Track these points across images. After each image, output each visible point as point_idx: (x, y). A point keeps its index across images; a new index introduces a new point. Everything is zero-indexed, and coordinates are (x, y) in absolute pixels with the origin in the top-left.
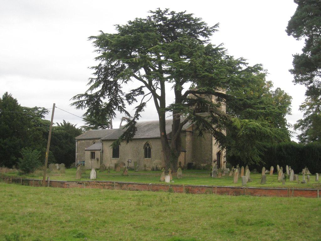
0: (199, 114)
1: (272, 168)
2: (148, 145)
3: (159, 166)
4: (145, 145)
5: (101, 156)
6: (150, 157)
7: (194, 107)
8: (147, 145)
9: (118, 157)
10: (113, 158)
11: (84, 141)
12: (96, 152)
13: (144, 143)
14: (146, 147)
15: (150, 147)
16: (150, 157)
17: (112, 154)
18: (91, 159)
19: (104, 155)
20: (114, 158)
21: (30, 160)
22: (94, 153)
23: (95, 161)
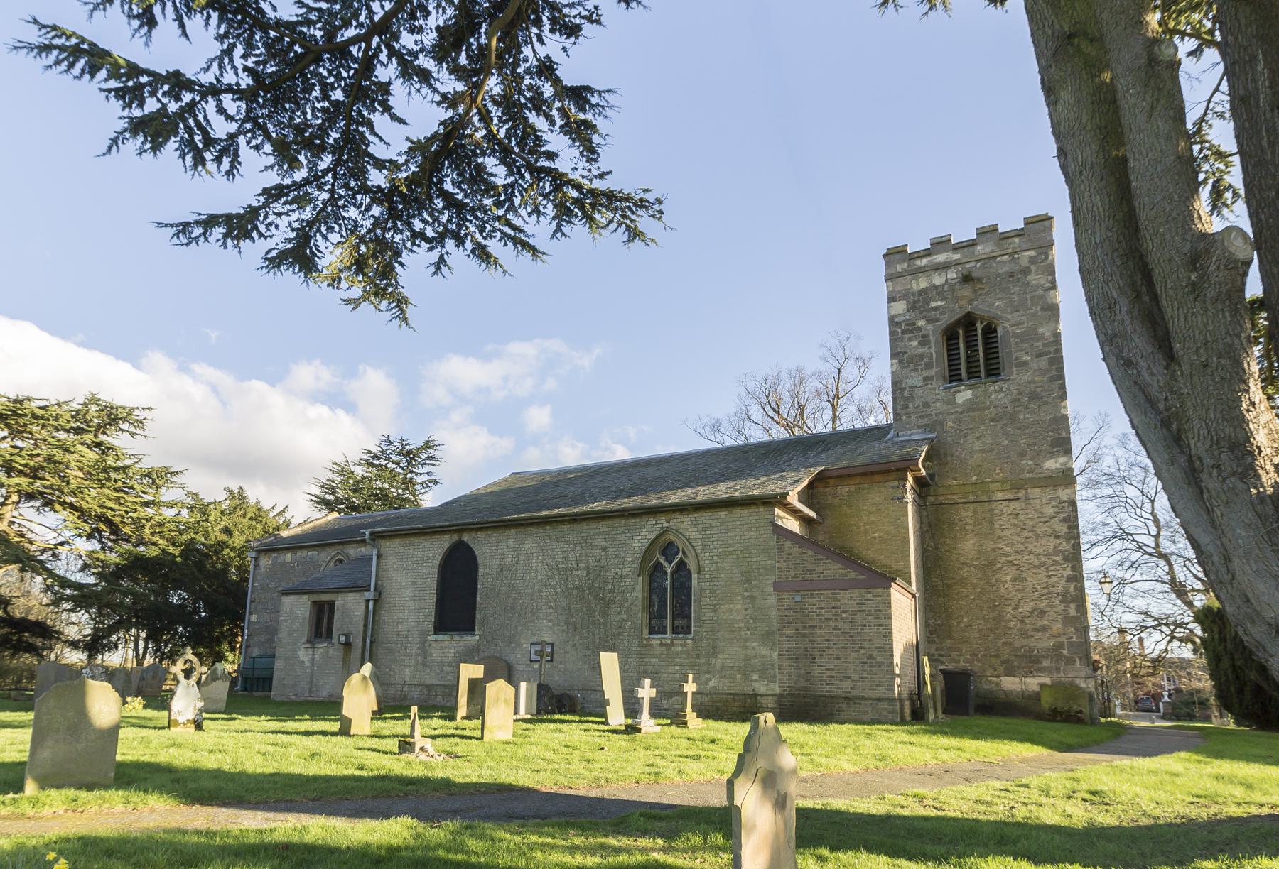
0: (429, 219)
1: (254, 234)
2: (669, 550)
3: (844, 706)
4: (649, 550)
5: (365, 626)
6: (683, 627)
7: (405, 191)
8: (663, 553)
9: (470, 629)
10: (435, 633)
11: (288, 557)
12: (340, 600)
13: (441, 545)
14: (658, 566)
15: (682, 565)
16: (683, 627)
17: (431, 610)
18: (308, 641)
19: (385, 615)
20: (440, 637)
21: (1073, 606)
22: (332, 605)
23: (331, 651)
